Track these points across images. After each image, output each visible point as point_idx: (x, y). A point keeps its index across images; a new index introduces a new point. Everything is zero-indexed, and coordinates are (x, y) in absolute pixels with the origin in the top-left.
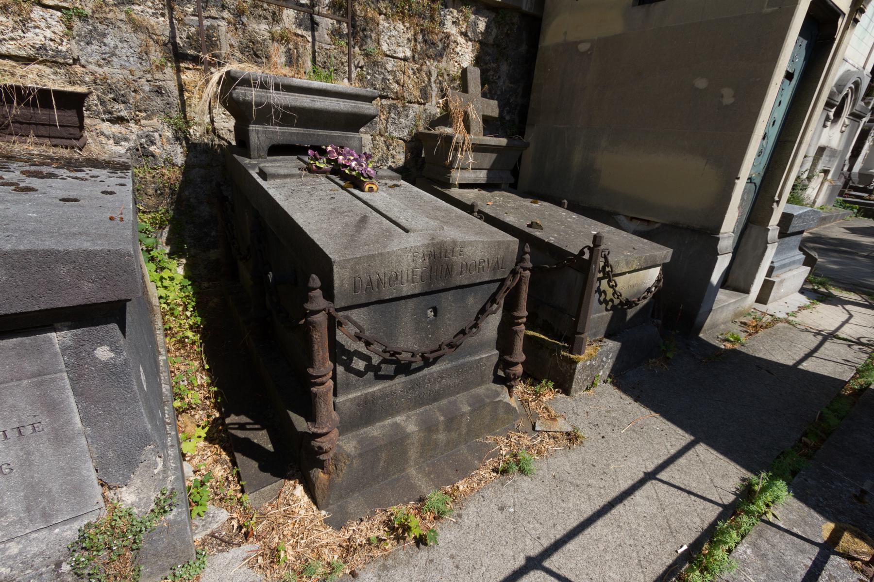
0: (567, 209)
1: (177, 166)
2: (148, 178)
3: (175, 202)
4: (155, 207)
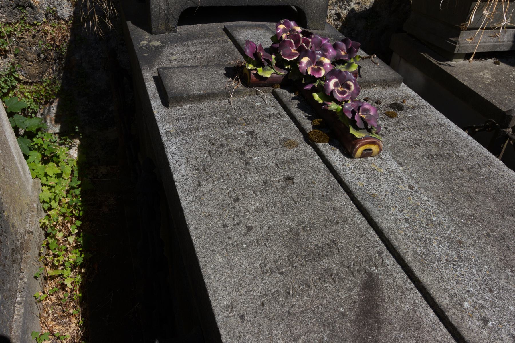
1: (64, 20)
2: (27, 38)
3: (64, 69)
4: (38, 77)
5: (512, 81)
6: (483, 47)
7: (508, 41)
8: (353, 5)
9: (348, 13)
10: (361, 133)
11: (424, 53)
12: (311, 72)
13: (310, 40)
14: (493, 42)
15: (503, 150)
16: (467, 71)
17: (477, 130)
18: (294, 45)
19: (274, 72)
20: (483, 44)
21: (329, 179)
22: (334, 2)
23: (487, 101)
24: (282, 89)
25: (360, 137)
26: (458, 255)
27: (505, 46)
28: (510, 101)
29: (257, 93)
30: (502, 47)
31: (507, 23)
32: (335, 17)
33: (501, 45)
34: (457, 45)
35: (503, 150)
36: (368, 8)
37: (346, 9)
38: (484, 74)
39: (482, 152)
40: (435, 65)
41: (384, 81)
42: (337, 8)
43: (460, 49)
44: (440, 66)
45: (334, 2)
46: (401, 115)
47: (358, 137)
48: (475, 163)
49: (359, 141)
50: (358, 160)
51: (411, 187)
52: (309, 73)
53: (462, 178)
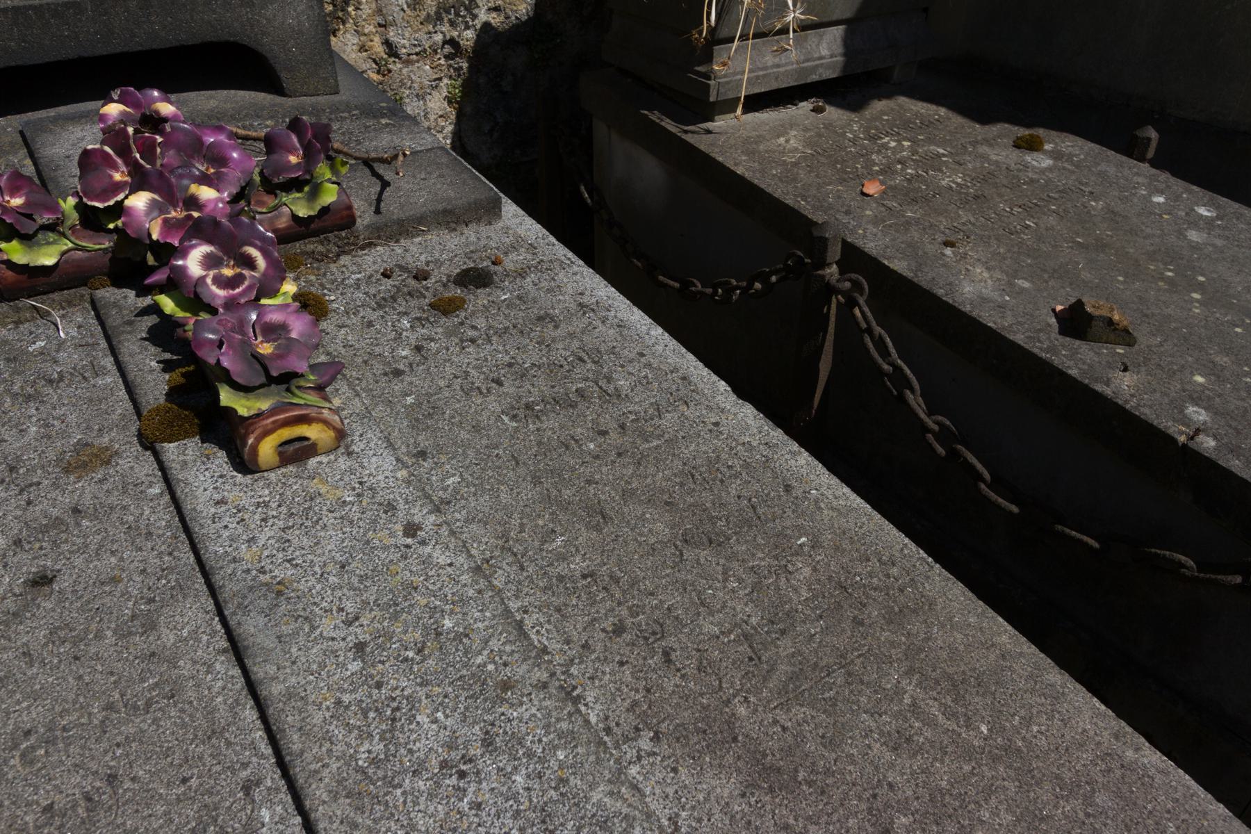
0: (1154, 164)
5: (851, 147)
6: (777, 78)
7: (832, 56)
8: (483, 16)
9: (477, 36)
10: (258, 398)
11: (650, 110)
12: (161, 234)
13: (159, 139)
14: (798, 63)
15: (833, 319)
16: (747, 141)
17: (774, 279)
18: (119, 161)
19: (70, 245)
20: (775, 70)
21: (170, 554)
22: (432, 13)
23: (787, 205)
24: (119, 286)
25: (252, 412)
26: (487, 733)
27: (828, 67)
28: (839, 197)
29: (44, 315)
30: (821, 70)
31: (797, 15)
32: (448, 49)
33: (817, 66)
34: (712, 83)
35: (833, 319)
36: (525, 18)
37: (467, 27)
38: (787, 141)
39: (678, 365)
40: (674, 135)
41: (445, 212)
42: (446, 28)
43: (722, 90)
44: (684, 137)
45: (432, 13)
46: (481, 298)
47: (246, 414)
48: (646, 404)
49: (252, 424)
50: (272, 476)
51: (411, 529)
52: (155, 237)
53: (597, 457)
